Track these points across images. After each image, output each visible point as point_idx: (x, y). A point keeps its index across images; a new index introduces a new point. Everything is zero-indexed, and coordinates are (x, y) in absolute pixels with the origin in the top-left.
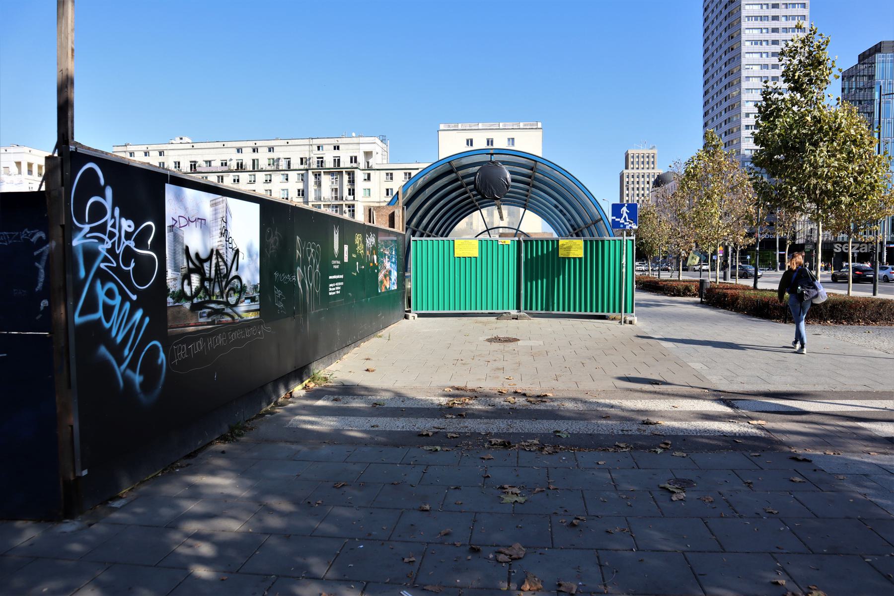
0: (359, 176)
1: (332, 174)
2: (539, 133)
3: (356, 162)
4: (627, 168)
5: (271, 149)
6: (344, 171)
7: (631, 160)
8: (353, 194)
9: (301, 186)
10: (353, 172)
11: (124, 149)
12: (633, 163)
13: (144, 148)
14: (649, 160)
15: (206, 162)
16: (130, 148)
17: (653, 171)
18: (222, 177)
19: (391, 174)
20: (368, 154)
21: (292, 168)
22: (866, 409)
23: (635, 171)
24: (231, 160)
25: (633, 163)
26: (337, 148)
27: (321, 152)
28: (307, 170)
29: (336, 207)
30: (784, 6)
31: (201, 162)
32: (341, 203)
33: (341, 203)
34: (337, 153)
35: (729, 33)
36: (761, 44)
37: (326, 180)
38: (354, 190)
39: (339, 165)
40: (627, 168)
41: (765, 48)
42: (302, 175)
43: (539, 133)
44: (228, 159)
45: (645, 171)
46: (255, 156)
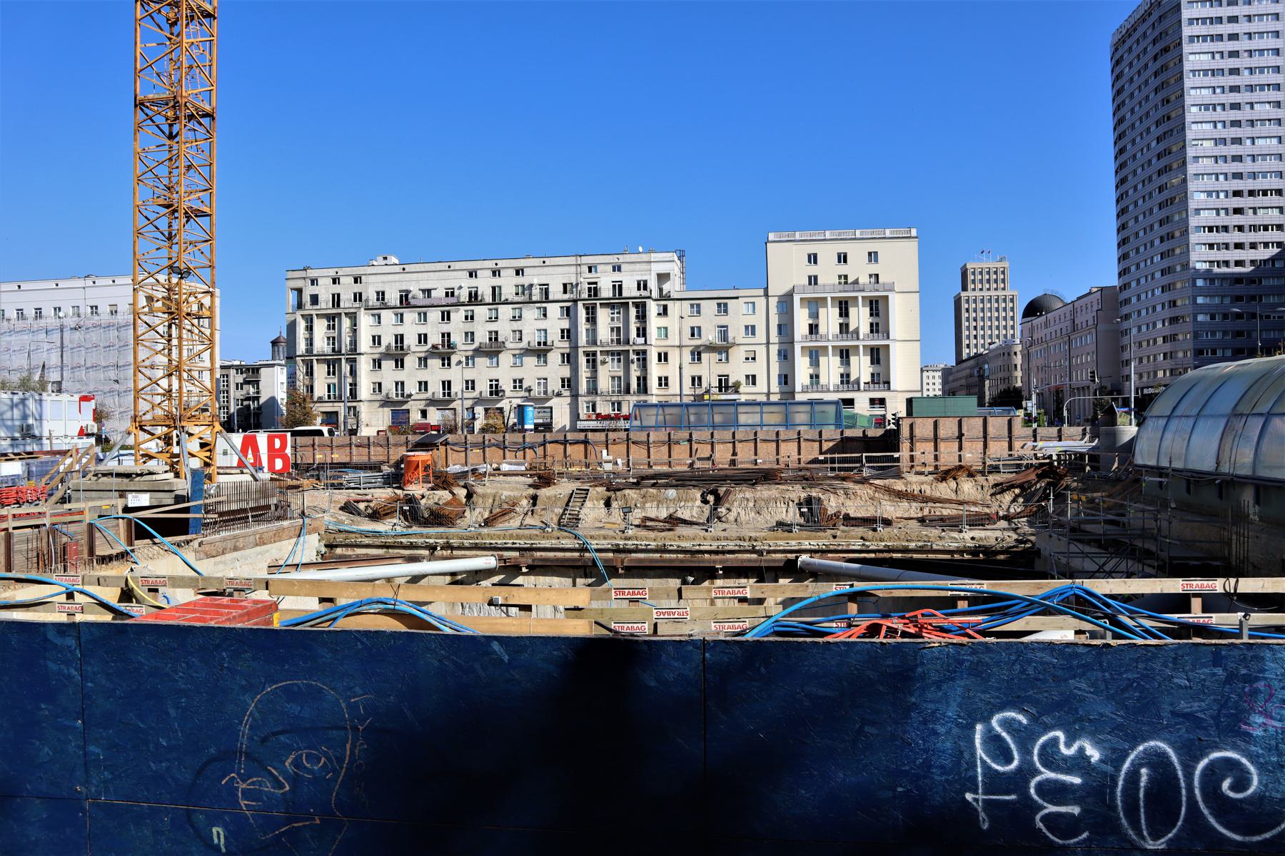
0: (653, 308)
1: (612, 306)
2: (914, 245)
3: (645, 288)
4: (965, 288)
5: (519, 272)
6: (630, 301)
7: (971, 277)
8: (644, 335)
9: (565, 324)
10: (644, 305)
11: (302, 274)
12: (973, 282)
13: (332, 272)
14: (998, 278)
15: (424, 291)
16: (312, 273)
18: (449, 313)
19: (698, 306)
20: (663, 278)
21: (551, 298)
22: (560, 555)
23: (978, 293)
24: (460, 288)
26: (617, 268)
27: (593, 274)
28: (575, 301)
29: (619, 353)
30: (1246, 54)
31: (415, 289)
32: (626, 348)
33: (626, 348)
34: (617, 276)
36: (1214, 110)
37: (603, 316)
38: (644, 329)
39: (620, 293)
40: (965, 288)
41: (1220, 114)
42: (568, 308)
43: (914, 245)
44: (456, 286)
46: (496, 281)
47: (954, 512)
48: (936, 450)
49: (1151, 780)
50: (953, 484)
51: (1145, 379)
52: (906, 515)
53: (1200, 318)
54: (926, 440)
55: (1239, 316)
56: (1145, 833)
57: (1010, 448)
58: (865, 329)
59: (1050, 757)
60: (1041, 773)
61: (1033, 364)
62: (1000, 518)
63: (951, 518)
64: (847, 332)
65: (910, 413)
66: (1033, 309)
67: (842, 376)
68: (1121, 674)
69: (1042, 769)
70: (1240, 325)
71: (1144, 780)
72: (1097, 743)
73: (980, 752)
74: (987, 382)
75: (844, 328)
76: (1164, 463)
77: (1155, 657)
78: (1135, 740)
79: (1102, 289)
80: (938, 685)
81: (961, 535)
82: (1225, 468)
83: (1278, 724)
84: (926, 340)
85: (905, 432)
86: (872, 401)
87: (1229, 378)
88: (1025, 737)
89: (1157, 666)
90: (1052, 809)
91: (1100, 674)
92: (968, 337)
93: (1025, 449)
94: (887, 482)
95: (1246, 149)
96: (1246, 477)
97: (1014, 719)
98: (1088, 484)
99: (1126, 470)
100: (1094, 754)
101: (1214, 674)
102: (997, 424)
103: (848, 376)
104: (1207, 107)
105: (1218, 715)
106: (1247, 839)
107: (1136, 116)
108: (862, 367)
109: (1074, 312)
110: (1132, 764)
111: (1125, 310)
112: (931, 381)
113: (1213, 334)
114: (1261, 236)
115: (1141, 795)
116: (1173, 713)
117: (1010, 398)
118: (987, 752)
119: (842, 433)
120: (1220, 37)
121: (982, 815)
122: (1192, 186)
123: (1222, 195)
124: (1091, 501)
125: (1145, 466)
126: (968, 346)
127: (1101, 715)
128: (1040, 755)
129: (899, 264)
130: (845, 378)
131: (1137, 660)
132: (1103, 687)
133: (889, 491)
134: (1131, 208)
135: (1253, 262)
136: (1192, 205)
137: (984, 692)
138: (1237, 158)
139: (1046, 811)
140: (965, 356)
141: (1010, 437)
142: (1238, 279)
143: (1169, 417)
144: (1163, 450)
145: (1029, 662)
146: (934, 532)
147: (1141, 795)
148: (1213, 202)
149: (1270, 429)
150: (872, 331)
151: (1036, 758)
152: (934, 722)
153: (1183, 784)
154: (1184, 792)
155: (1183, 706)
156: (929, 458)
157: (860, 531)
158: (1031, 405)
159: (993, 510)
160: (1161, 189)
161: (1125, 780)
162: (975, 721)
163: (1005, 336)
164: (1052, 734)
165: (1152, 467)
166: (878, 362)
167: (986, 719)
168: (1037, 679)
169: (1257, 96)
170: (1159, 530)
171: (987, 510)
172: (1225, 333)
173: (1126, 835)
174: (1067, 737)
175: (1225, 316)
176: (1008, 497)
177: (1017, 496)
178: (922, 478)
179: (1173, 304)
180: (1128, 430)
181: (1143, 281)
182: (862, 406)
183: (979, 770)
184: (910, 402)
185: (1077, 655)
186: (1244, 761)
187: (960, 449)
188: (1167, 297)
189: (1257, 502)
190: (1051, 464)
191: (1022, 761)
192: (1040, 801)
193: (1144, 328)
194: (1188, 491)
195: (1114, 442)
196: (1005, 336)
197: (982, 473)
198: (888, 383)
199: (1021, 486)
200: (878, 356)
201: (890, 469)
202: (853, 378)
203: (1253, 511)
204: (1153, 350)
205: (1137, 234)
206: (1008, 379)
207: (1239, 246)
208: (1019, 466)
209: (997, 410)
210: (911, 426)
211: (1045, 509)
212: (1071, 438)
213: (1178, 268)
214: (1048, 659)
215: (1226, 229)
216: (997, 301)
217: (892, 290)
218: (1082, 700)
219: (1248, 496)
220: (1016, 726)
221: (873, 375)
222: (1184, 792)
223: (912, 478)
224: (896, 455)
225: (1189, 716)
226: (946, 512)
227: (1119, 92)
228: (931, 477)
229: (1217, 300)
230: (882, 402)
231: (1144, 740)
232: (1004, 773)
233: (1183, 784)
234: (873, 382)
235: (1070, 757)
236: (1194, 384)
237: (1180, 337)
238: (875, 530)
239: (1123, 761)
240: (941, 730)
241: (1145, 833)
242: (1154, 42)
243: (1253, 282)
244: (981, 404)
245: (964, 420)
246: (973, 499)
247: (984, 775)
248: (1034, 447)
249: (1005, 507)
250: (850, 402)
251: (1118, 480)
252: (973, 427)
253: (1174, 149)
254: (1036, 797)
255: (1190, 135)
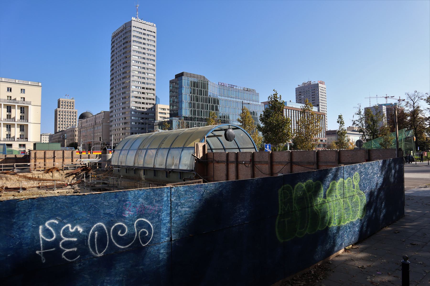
2: (40, 89)
4: (59, 107)
12: (62, 105)
14: (71, 105)
17: (73, 110)
23: (63, 109)
25: (62, 105)
35: (125, 55)
40: (59, 107)
41: (140, 65)
45: (66, 110)
47: (51, 184)
48: (45, 162)
49: (99, 235)
50: (51, 174)
51: (117, 141)
52: (32, 186)
53: (133, 123)
54: (41, 158)
55: (143, 123)
56: (97, 252)
57: (72, 161)
58: (18, 117)
59: (66, 233)
60: (63, 239)
61: (82, 135)
62: (68, 185)
63: (50, 186)
64: (10, 118)
65: (35, 149)
66: (82, 116)
67: (7, 135)
68: (88, 203)
69: (64, 238)
70: (143, 126)
71: (96, 235)
72: (82, 226)
73: (41, 236)
74: (66, 141)
75: (9, 117)
76: (120, 164)
77: (99, 197)
78: (93, 224)
79: (105, 112)
80: (25, 214)
81: (54, 192)
82: (136, 165)
83: (132, 213)
84: (43, 123)
85: (33, 155)
86: (20, 145)
87: (138, 138)
88: (57, 228)
89: (99, 200)
90: (67, 250)
91: (82, 204)
92: (59, 124)
93: (77, 162)
94: (24, 174)
95: (146, 76)
96: (141, 167)
97: (53, 222)
98: (98, 172)
99: (109, 167)
100: (81, 230)
101: (115, 201)
102: (68, 153)
103: (10, 135)
104: (137, 62)
105: (117, 213)
106: (125, 247)
107: (117, 60)
108: (16, 132)
109: (96, 118)
110: (93, 231)
111: (111, 119)
112: (45, 139)
113: (136, 128)
114: (149, 101)
115: (96, 240)
116: (104, 213)
117: (74, 146)
118: (44, 235)
119: (5, 156)
120: (141, 43)
121: (43, 258)
122: (132, 84)
123: (139, 88)
124: (98, 177)
125: (114, 165)
126: (59, 127)
127: (83, 217)
128: (63, 233)
129: (34, 95)
130: (9, 136)
131: (93, 198)
132: (83, 208)
133: (25, 177)
134: (114, 87)
135: (147, 108)
136: (131, 90)
137: (42, 214)
138: (144, 78)
139: (65, 252)
140: (58, 131)
141: (72, 158)
142: (143, 113)
143: (121, 150)
144: (119, 160)
145: (58, 202)
146: (43, 191)
147: (96, 240)
148: (137, 89)
149: (147, 153)
150: (21, 119)
151: (61, 234)
152: (23, 228)
153: (107, 235)
154: (108, 237)
155: (107, 211)
156: (42, 165)
157: (13, 193)
158: (80, 148)
159: (66, 183)
160: (123, 83)
161: (91, 237)
162: (39, 225)
163: (73, 125)
164: (66, 226)
165: (116, 166)
166: (23, 131)
167: (43, 224)
168: (61, 208)
169: (149, 62)
170: (118, 184)
171: (64, 183)
172: (139, 128)
173: (91, 254)
174: (72, 226)
175: (139, 123)
176: (71, 178)
177: (74, 177)
178: (39, 172)
179: (125, 118)
180: (110, 155)
181: (117, 110)
182: (16, 146)
183: (41, 242)
184: (35, 145)
185: (74, 199)
186: (124, 225)
187: (54, 161)
188: (123, 116)
189: (144, 174)
190: (86, 166)
191: (57, 236)
192: (63, 249)
193: (117, 125)
194: (126, 172)
195: (106, 159)
196: (73, 125)
197: (62, 170)
198: (27, 138)
199: (75, 174)
200: (23, 128)
201: (25, 169)
202: (12, 136)
203: (143, 177)
204: (119, 132)
205: (116, 96)
206: (73, 139)
207: (143, 103)
208: (75, 167)
209: (68, 148)
210: (35, 153)
211: (83, 181)
212: (93, 158)
213: (127, 108)
214: (65, 201)
215: (140, 98)
216: (70, 113)
217: (30, 104)
218: (76, 213)
219: (142, 172)
220: (54, 225)
221: (21, 135)
222: (108, 237)
223: (35, 172)
224: (29, 164)
225: (109, 214)
226: (48, 184)
227: (113, 51)
228: (42, 172)
229: (137, 118)
230: (24, 146)
231: (96, 223)
232: (50, 242)
233: (107, 235)
234: (21, 138)
235: (73, 232)
236: (129, 140)
237: (127, 129)
238: (19, 192)
239: (90, 231)
240: (26, 230)
241: (97, 252)
242: (124, 39)
243: (146, 114)
244: (63, 145)
245: (56, 152)
246: (58, 179)
247: (43, 243)
248: (80, 161)
249: (70, 181)
250: (10, 145)
251: (107, 171)
252: (59, 154)
253: (127, 72)
254: (62, 248)
255: (132, 69)
